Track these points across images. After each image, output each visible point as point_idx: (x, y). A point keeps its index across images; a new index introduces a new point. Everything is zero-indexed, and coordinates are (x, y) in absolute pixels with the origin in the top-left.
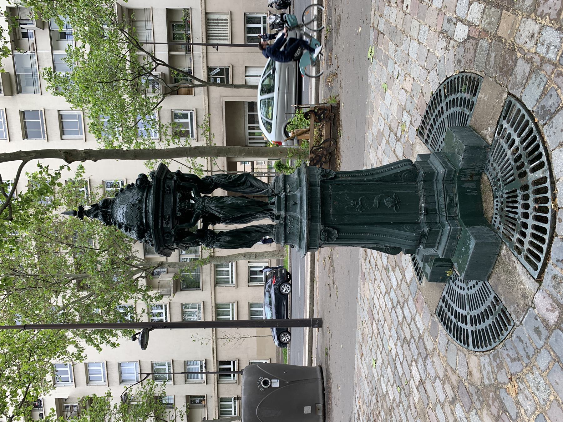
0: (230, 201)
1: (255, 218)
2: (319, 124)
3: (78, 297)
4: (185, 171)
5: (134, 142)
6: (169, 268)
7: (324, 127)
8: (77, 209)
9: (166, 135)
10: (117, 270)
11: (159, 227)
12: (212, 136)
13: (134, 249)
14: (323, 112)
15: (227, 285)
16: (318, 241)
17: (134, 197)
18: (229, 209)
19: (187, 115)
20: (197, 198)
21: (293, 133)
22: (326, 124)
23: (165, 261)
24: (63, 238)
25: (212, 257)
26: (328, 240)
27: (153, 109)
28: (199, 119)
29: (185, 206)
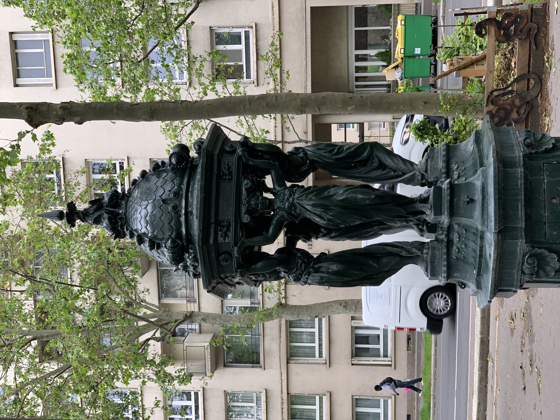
0: (342, 194)
1: (387, 229)
2: (505, 45)
3: (41, 372)
4: (256, 137)
5: (144, 88)
6: (203, 324)
7: (516, 51)
8: (64, 208)
9: (200, 75)
10: (110, 325)
11: (211, 241)
12: (285, 76)
13: (140, 287)
14: (514, 22)
15: (311, 360)
16: (516, 275)
17: (164, 187)
18: (338, 209)
19: (240, 37)
20: (278, 188)
21: (451, 64)
22: (521, 44)
23: (197, 310)
24: (17, 265)
25: (282, 306)
26: (539, 274)
27: (179, 26)
28: (261, 43)
29: (257, 205)
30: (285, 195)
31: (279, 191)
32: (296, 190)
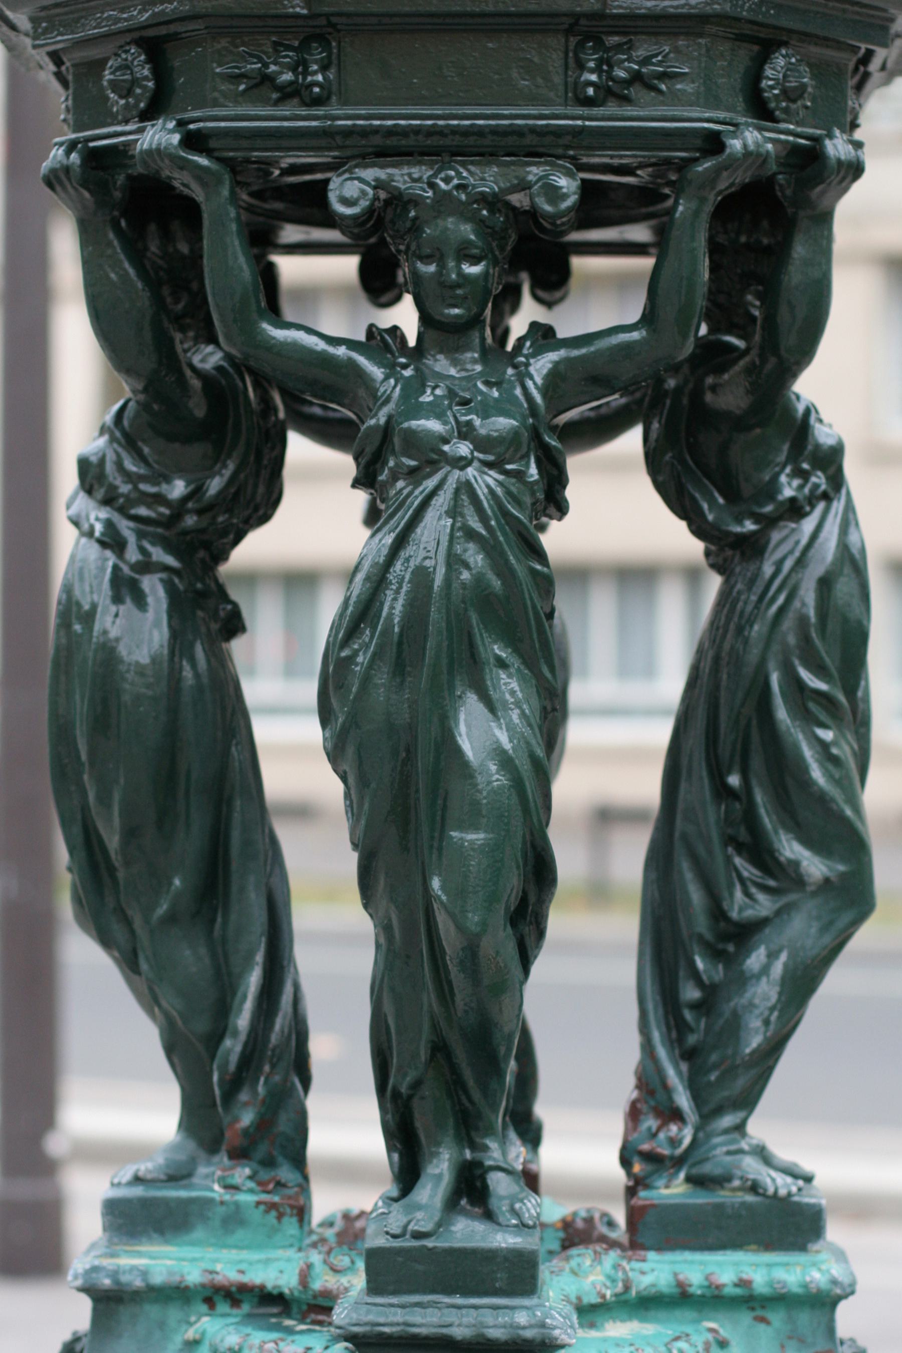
30: (485, 413)
31: (523, 375)
32: (519, 475)
